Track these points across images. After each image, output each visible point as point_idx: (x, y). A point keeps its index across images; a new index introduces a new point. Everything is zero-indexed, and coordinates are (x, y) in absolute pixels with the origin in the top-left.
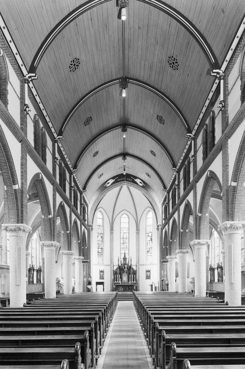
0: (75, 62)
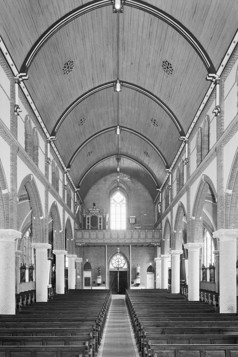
0: (69, 64)
